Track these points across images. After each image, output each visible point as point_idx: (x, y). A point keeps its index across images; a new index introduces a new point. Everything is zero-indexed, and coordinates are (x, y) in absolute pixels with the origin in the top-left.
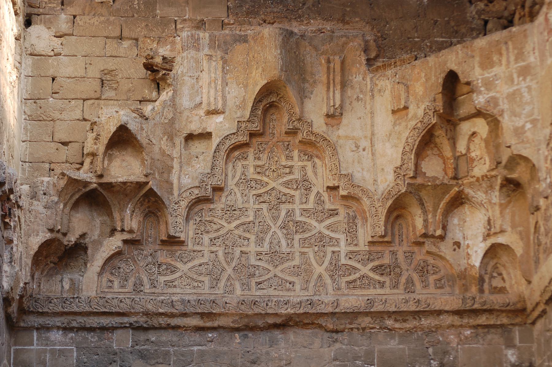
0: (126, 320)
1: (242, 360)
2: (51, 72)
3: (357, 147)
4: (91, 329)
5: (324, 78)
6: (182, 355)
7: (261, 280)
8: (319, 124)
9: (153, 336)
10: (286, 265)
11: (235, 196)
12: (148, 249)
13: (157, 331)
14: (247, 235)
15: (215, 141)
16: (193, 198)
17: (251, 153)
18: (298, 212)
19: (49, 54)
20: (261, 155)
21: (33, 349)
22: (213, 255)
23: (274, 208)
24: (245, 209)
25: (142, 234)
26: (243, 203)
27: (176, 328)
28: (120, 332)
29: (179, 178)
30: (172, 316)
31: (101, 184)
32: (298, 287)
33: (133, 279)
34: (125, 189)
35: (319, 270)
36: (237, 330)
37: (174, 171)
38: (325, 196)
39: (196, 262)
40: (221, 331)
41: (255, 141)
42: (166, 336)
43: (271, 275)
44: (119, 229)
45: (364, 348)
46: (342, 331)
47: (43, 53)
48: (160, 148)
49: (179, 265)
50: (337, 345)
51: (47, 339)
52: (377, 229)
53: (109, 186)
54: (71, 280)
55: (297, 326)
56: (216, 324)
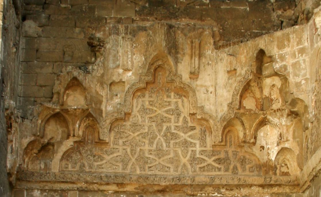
18: (173, 128)
23: (159, 126)
29: (106, 107)
31: (62, 110)
38: (189, 119)
39: (115, 155)
52: (217, 138)
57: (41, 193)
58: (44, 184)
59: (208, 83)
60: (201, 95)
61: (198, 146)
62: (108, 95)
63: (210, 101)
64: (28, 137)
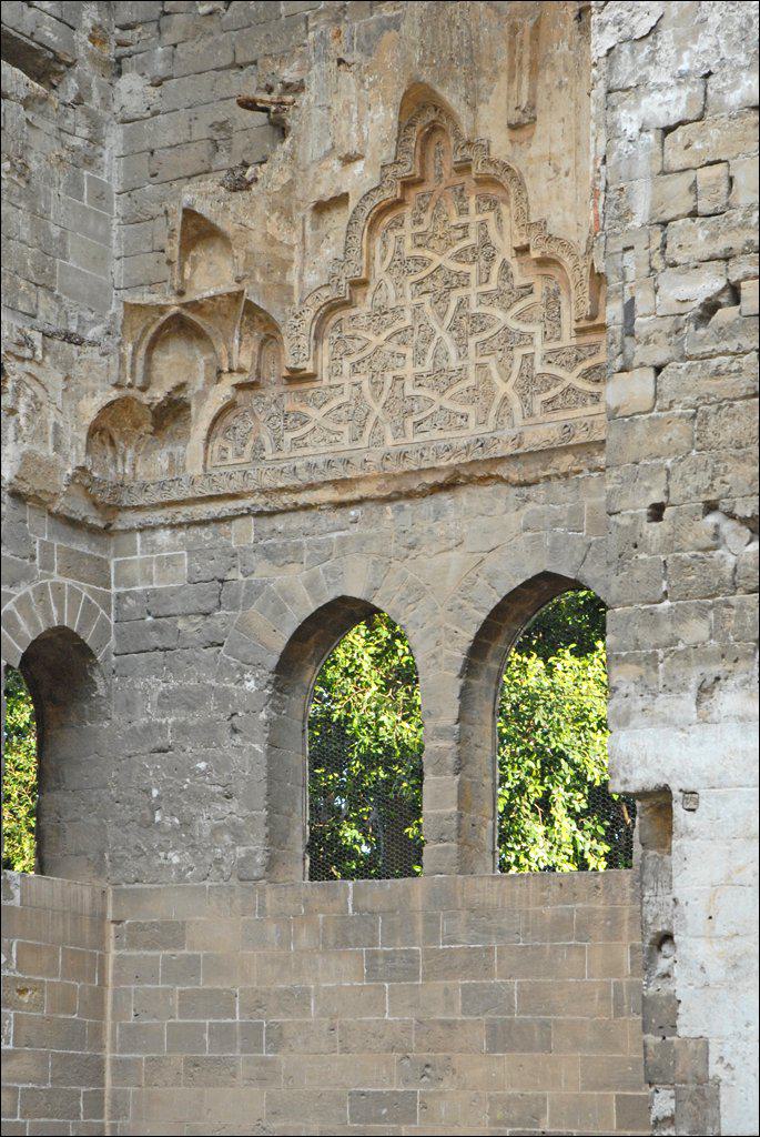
0: (240, 504)
1: (397, 545)
2: (147, 144)
3: (557, 171)
4: (203, 523)
5: (503, 60)
6: (318, 547)
7: (420, 418)
8: (501, 145)
9: (279, 523)
10: (457, 388)
11: (388, 288)
12: (271, 393)
13: (286, 516)
14: (402, 350)
15: (353, 203)
16: (322, 304)
17: (408, 212)
18: (473, 300)
19: (145, 115)
20: (423, 216)
21: (135, 560)
22: (356, 389)
23: (440, 299)
24: (399, 309)
25: (258, 372)
26: (397, 298)
27: (307, 507)
28: (239, 522)
29: (301, 276)
30: (296, 490)
31: (184, 306)
32: (472, 420)
33: (251, 442)
34: (219, 308)
35: (504, 388)
36: (388, 500)
37: (294, 267)
38: (514, 265)
39: (334, 404)
40: (369, 505)
41: (413, 194)
42: (299, 521)
43: (435, 408)
44: (226, 369)
45: (568, 505)
46: (536, 482)
47: (137, 116)
48: (265, 235)
49: (312, 412)
50: (530, 506)
51: (153, 543)
52: (582, 307)
53: (195, 306)
54: (171, 454)
55: (471, 482)
56: (356, 495)
57: (174, 535)
58: (174, 510)
59: (559, 146)
60: (539, 188)
61: (538, 340)
62: (308, 242)
63: (563, 199)
64: (99, 393)
